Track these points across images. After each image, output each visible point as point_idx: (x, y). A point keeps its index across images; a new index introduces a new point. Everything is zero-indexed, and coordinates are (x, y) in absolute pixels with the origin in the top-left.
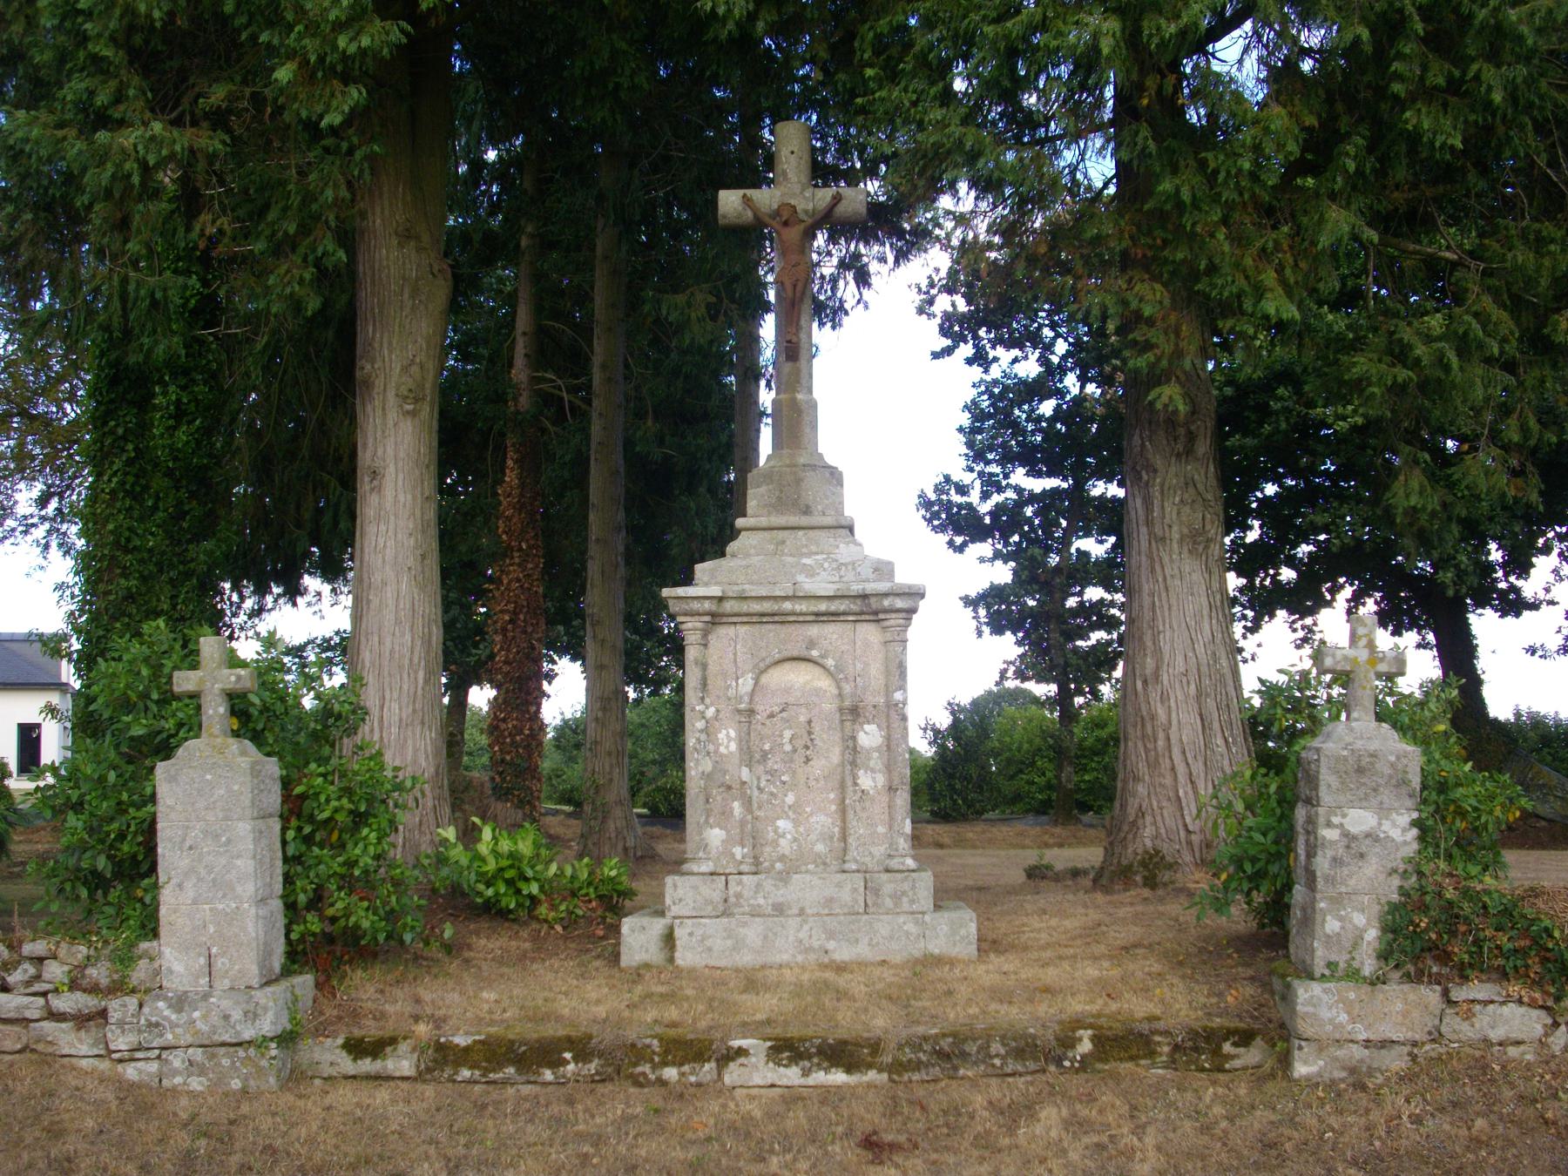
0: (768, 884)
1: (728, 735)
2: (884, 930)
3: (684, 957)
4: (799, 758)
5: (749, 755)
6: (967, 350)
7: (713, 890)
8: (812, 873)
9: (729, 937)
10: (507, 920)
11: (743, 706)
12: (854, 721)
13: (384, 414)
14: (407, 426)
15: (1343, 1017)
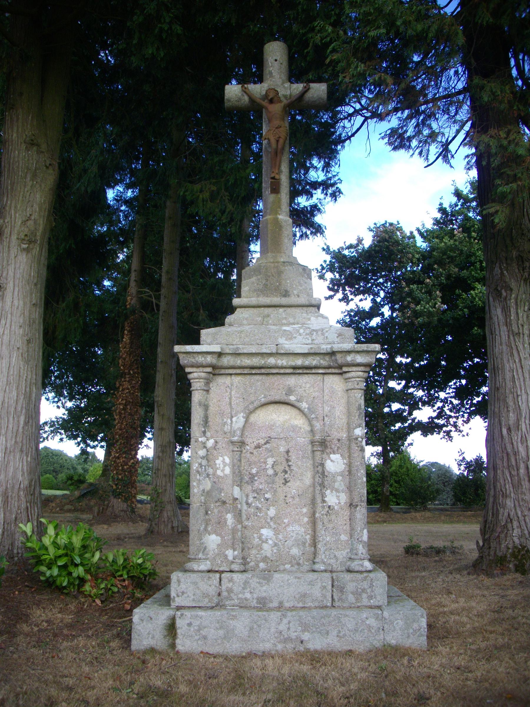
0: (254, 582)
1: (223, 461)
2: (350, 624)
3: (185, 644)
4: (279, 480)
5: (240, 478)
6: (340, 295)
7: (209, 585)
8: (289, 572)
9: (221, 628)
10: (62, 593)
11: (236, 439)
12: (323, 451)
13: (9, 251)
14: (23, 258)
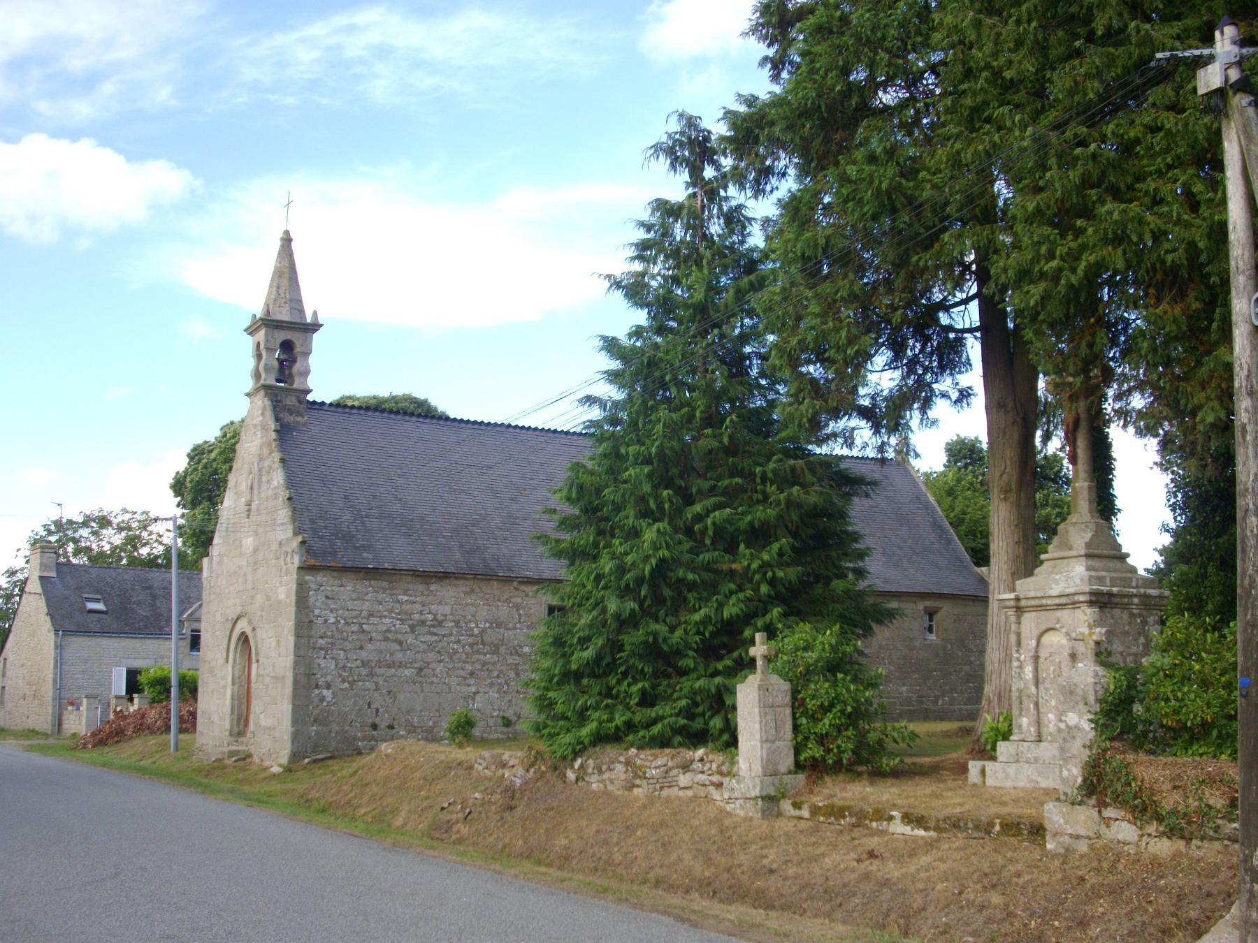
15: (1062, 821)
